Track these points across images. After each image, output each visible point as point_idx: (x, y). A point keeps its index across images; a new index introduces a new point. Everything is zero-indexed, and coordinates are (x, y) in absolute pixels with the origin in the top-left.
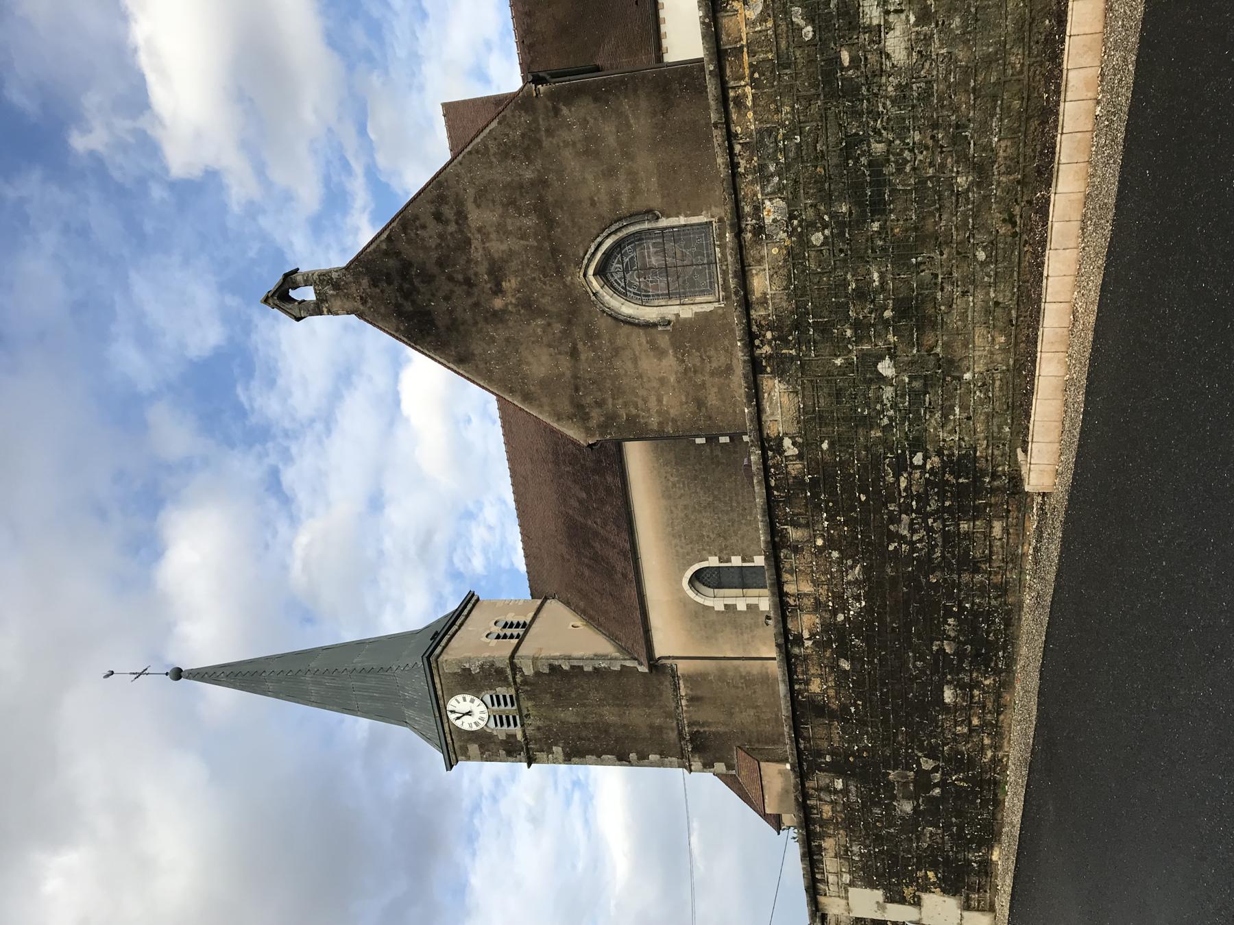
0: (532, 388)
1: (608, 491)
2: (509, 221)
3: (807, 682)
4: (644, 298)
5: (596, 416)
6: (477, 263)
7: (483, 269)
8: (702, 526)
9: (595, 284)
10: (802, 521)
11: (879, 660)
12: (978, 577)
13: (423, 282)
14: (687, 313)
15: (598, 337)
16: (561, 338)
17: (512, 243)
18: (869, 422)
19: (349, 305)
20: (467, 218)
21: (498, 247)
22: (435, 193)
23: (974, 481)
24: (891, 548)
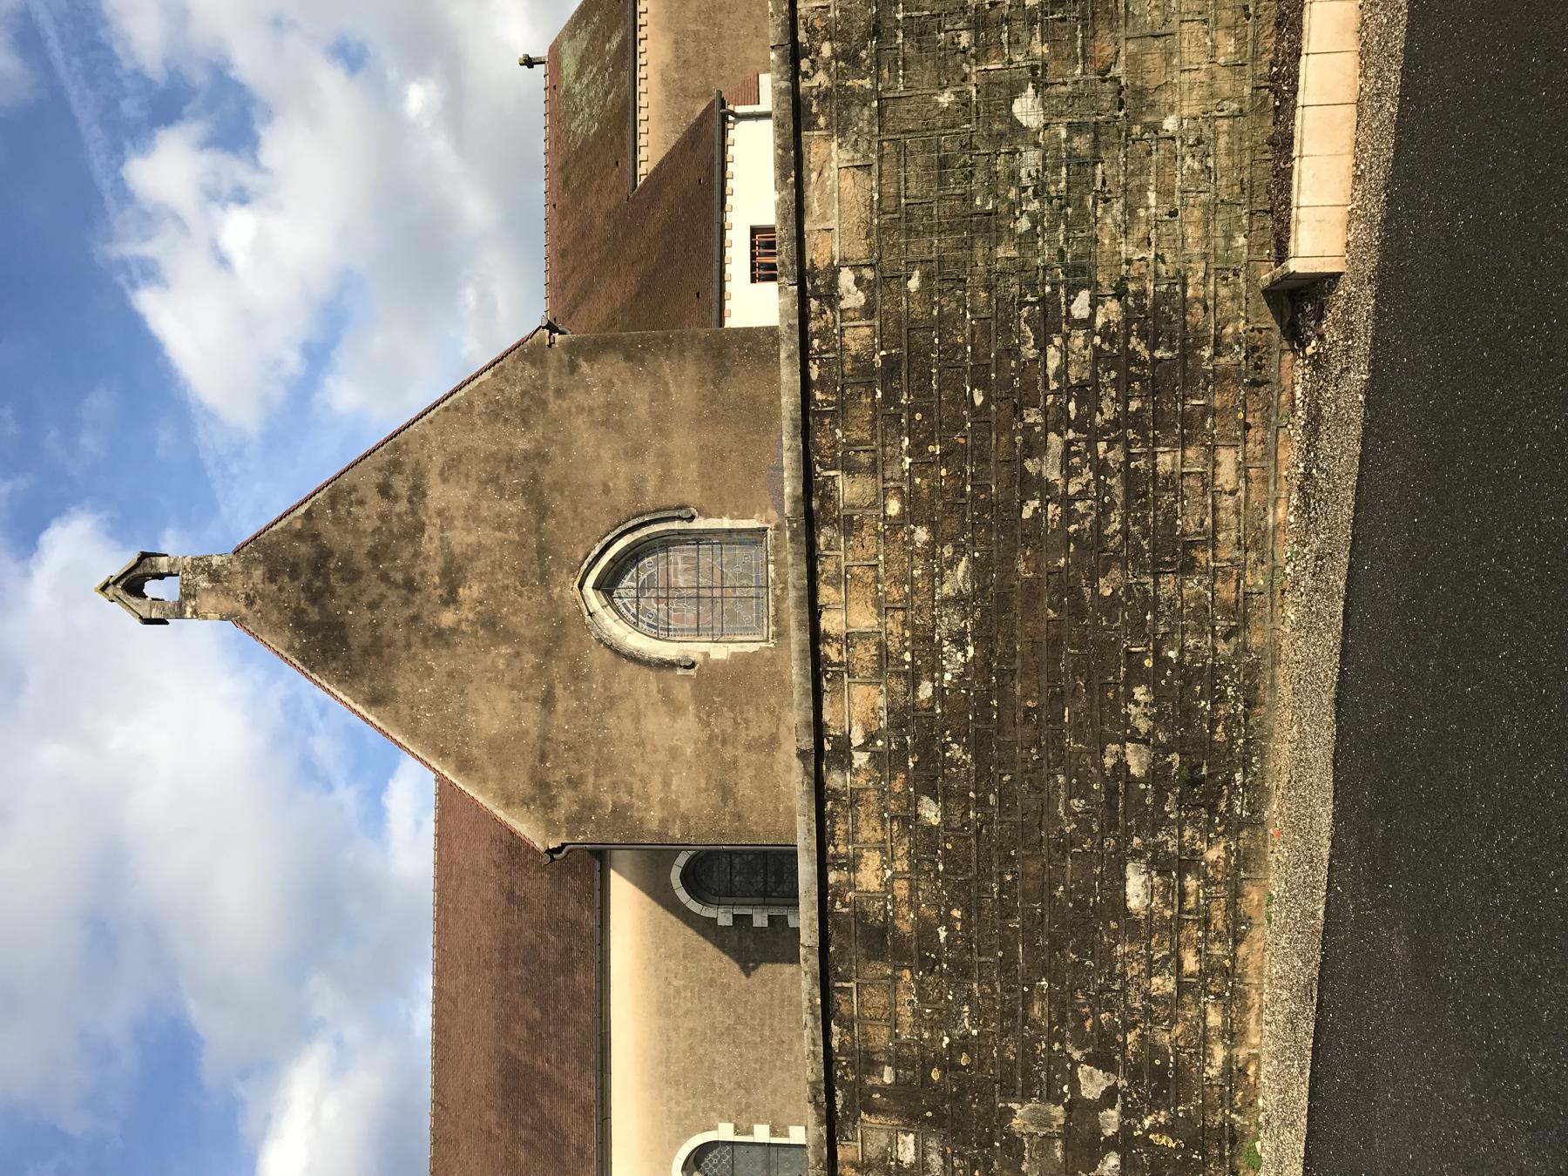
0: (475, 751)
1: (575, 1000)
2: (484, 504)
3: (853, 864)
4: (661, 630)
5: (566, 803)
6: (427, 559)
7: (434, 568)
8: (714, 1066)
9: (594, 601)
10: (864, 458)
11: (1000, 797)
12: (1192, 585)
13: (343, 580)
14: (720, 652)
15: (588, 678)
16: (531, 677)
17: (484, 535)
18: (990, 226)
19: (227, 605)
20: (425, 495)
21: (461, 538)
22: (387, 458)
23: (1184, 356)
24: (1027, 513)
